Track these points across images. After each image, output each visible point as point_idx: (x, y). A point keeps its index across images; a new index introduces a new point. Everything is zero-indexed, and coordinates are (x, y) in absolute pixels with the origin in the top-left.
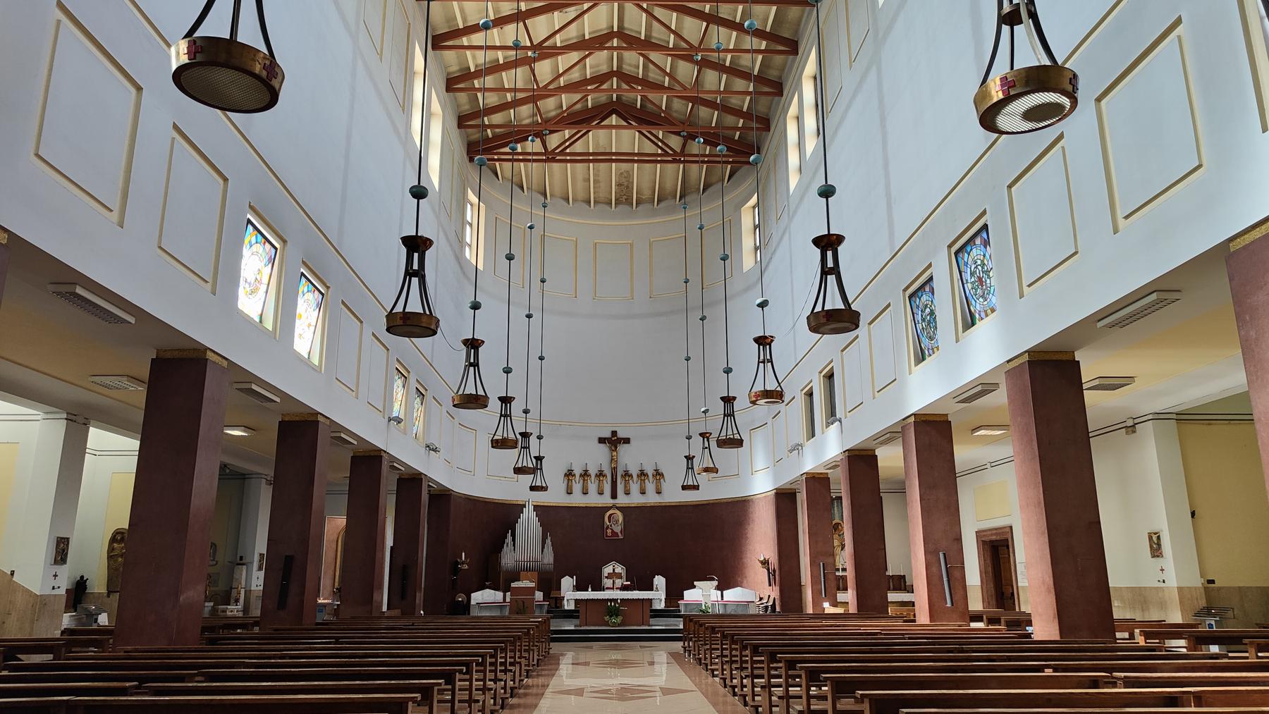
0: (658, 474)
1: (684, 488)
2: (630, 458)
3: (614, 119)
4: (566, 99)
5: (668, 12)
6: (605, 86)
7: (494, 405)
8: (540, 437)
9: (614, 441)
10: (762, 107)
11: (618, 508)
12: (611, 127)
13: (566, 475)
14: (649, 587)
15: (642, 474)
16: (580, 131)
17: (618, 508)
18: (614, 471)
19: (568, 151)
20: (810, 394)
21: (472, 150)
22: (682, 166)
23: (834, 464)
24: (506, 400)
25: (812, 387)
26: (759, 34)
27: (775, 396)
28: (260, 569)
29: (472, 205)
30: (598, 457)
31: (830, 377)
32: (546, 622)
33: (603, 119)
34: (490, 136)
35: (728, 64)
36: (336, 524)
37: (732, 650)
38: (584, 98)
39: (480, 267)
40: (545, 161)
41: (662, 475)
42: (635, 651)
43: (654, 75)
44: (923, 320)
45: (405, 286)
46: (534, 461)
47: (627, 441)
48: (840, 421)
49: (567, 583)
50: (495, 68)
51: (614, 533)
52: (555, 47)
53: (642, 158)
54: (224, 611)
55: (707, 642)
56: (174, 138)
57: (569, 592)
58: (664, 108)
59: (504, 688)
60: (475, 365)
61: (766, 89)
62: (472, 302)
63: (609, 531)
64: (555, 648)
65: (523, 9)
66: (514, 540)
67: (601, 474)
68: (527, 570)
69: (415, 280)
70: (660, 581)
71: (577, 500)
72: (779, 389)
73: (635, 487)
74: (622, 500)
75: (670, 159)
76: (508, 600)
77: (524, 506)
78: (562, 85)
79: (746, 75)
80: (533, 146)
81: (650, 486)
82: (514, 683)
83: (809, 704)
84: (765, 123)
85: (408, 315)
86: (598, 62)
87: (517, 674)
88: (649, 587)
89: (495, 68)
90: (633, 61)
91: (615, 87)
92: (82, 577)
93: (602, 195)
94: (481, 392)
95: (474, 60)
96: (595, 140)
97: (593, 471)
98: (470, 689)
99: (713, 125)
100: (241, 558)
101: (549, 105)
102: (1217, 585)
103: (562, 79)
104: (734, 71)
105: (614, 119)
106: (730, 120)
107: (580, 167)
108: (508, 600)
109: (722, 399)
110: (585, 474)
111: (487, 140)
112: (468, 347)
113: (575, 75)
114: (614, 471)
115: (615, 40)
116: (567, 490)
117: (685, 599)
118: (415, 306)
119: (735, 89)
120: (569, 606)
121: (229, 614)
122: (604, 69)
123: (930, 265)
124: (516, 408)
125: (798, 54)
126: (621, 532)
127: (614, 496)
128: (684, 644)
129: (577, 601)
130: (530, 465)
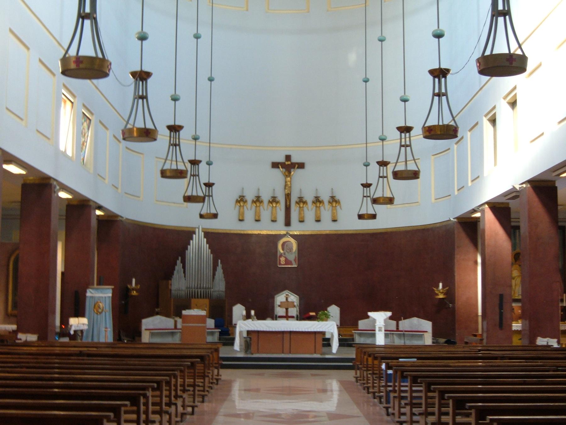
0: (334, 200)
1: (361, 217)
7: (164, 135)
8: (209, 164)
11: (294, 236)
13: (238, 201)
15: (317, 201)
18: (288, 196)
23: (514, 194)
24: (174, 129)
25: (516, 94)
41: (338, 202)
45: (78, 29)
46: (204, 187)
47: (301, 166)
49: (238, 310)
51: (287, 262)
55: (375, 372)
60: (144, 97)
62: (139, 33)
63: (283, 259)
64: (225, 374)
66: (184, 267)
67: (274, 200)
68: (198, 297)
69: (87, 23)
72: (452, 123)
74: (297, 229)
77: (194, 233)
81: (326, 213)
83: (439, 418)
85: (81, 59)
94: (150, 126)
97: (266, 198)
108: (179, 326)
110: (258, 200)
112: (137, 80)
114: (288, 196)
116: (239, 217)
117: (360, 328)
118: (88, 50)
123: (515, 88)
126: (295, 260)
127: (288, 223)
128: (356, 374)
130: (200, 194)
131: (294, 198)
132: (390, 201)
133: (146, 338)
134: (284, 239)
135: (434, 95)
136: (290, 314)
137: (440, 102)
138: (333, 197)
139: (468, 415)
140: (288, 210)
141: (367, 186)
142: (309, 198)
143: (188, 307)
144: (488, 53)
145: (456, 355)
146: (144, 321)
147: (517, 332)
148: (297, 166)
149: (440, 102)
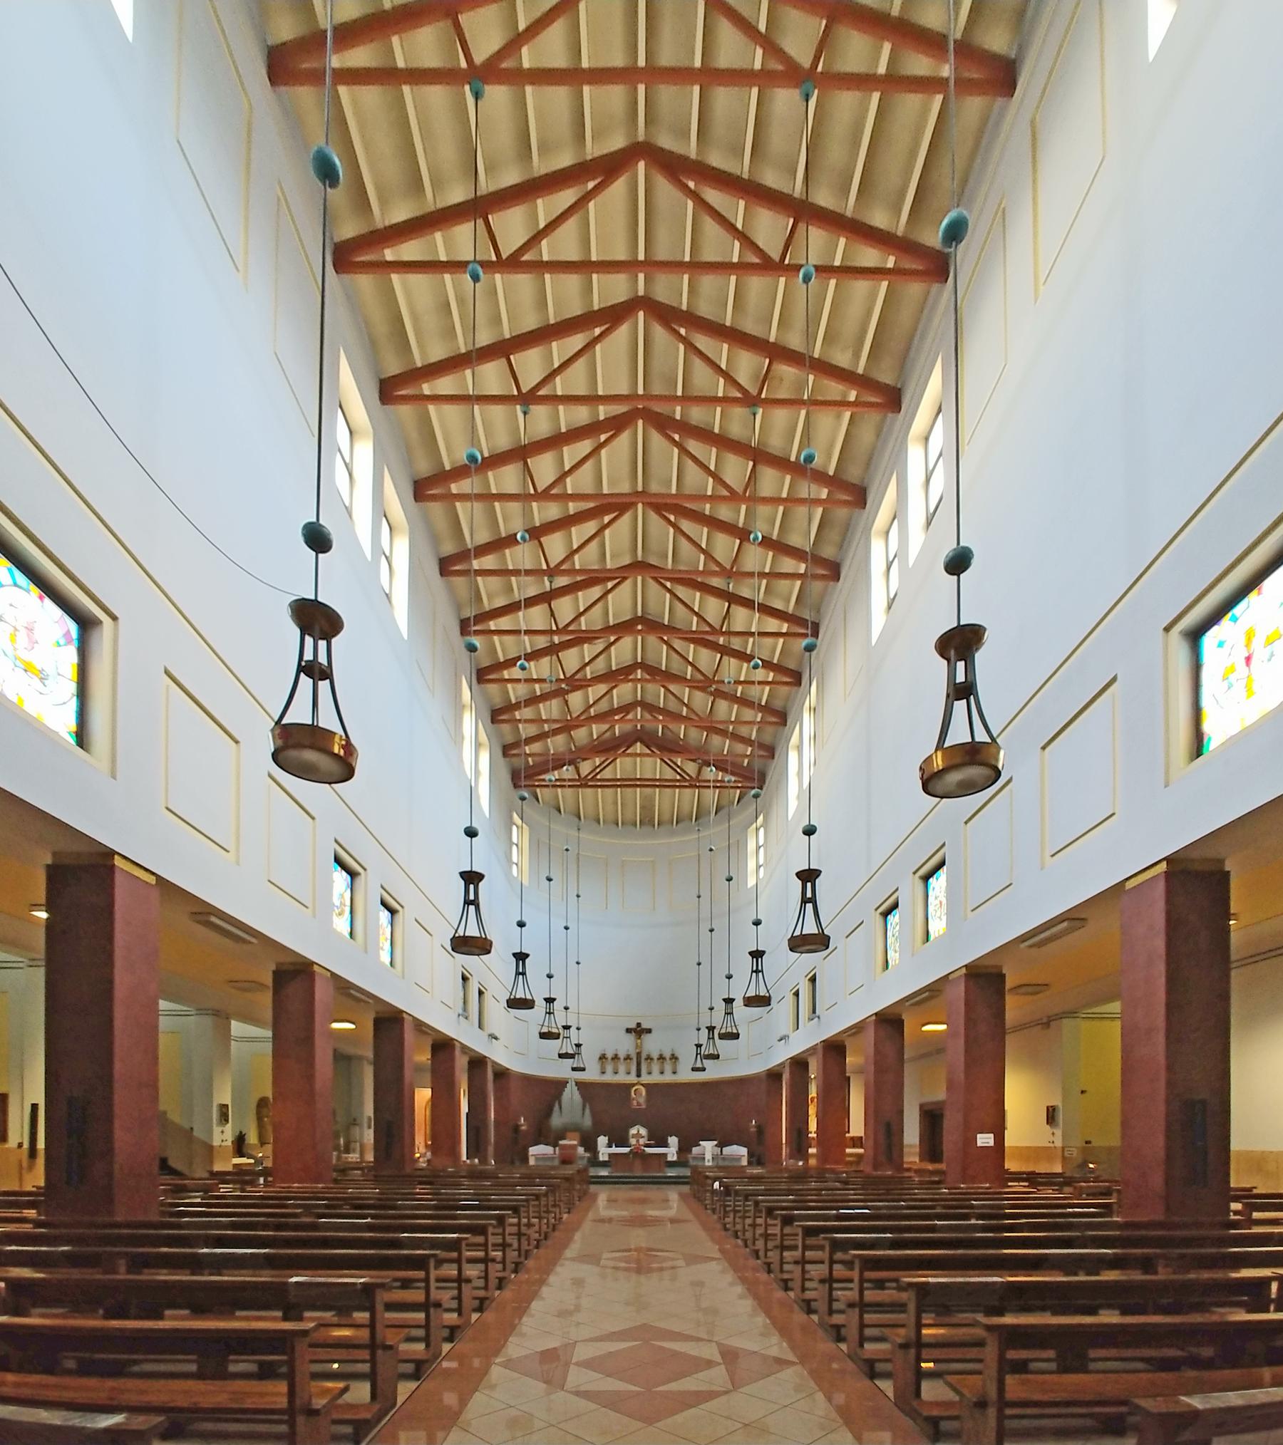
0: (674, 1058)
1: (693, 1069)
2: (652, 1045)
3: (638, 747)
4: (596, 729)
5: (690, 591)
6: (630, 716)
7: (540, 1004)
9: (639, 1031)
10: (767, 738)
12: (636, 680)
13: (600, 1058)
14: (666, 1145)
15: (661, 1058)
16: (607, 759)
17: (642, 1085)
18: (639, 1054)
19: (598, 777)
20: (797, 994)
21: (517, 778)
22: (697, 790)
24: (550, 1001)
26: (767, 665)
27: (761, 1001)
28: (369, 1127)
29: (517, 827)
30: (626, 1045)
31: (813, 980)
32: (585, 1170)
33: (628, 748)
34: (531, 763)
35: (739, 695)
36: (423, 1095)
37: (745, 1206)
38: (612, 727)
39: (525, 882)
40: (578, 786)
41: (676, 1059)
42: (652, 1192)
43: (673, 705)
44: (893, 936)
46: (574, 1047)
47: (649, 1031)
48: (819, 1017)
49: (602, 1141)
50: (533, 700)
51: (639, 1104)
52: (585, 679)
53: (662, 784)
54: (346, 1158)
56: (168, 686)
57: (604, 1149)
58: (682, 737)
59: (555, 1218)
61: (774, 720)
63: (635, 1103)
64: (593, 1188)
65: (557, 642)
66: (561, 1108)
69: (472, 908)
70: (673, 1141)
71: (609, 1078)
72: (767, 995)
73: (656, 1067)
74: (645, 1079)
75: (687, 784)
76: (557, 1152)
78: (592, 714)
79: (747, 741)
80: (567, 772)
81: (668, 1067)
82: (540, 1236)
84: (770, 751)
86: (623, 693)
87: (558, 1213)
88: (666, 1145)
89: (533, 700)
90: (657, 694)
91: (639, 717)
92: (241, 1132)
93: (629, 815)
95: (516, 692)
96: (621, 767)
98: (519, 1225)
99: (725, 753)
100: (355, 1120)
101: (580, 735)
102: (1094, 1144)
103: (588, 668)
104: (744, 702)
105: (638, 747)
106: (740, 748)
107: (609, 791)
108: (557, 1152)
109: (724, 1000)
110: (616, 1057)
111: (527, 767)
113: (603, 706)
114: (639, 1054)
115: (639, 671)
119: (745, 720)
120: (603, 1157)
121: (350, 1160)
122: (628, 699)
123: (897, 889)
124: (558, 1006)
125: (800, 685)
127: (639, 1075)
129: (610, 1155)
130: (570, 1051)
131: (644, 1056)
132: (717, 1057)
133: (532, 1162)
134: (636, 1087)
135: (753, 972)
136: (769, 1228)
137: (757, 976)
138: (673, 1055)
139: (776, 1219)
140: (639, 1064)
141: (699, 1046)
142: (655, 1056)
143: (563, 1138)
144: (797, 933)
145: (441, 1222)
146: (530, 1149)
147: (813, 1155)
148: (523, 704)
149: (757, 976)
